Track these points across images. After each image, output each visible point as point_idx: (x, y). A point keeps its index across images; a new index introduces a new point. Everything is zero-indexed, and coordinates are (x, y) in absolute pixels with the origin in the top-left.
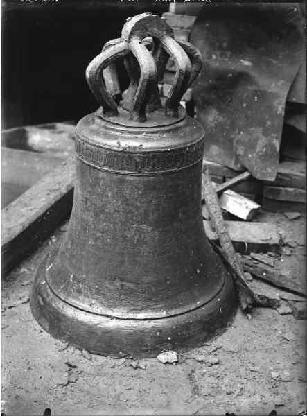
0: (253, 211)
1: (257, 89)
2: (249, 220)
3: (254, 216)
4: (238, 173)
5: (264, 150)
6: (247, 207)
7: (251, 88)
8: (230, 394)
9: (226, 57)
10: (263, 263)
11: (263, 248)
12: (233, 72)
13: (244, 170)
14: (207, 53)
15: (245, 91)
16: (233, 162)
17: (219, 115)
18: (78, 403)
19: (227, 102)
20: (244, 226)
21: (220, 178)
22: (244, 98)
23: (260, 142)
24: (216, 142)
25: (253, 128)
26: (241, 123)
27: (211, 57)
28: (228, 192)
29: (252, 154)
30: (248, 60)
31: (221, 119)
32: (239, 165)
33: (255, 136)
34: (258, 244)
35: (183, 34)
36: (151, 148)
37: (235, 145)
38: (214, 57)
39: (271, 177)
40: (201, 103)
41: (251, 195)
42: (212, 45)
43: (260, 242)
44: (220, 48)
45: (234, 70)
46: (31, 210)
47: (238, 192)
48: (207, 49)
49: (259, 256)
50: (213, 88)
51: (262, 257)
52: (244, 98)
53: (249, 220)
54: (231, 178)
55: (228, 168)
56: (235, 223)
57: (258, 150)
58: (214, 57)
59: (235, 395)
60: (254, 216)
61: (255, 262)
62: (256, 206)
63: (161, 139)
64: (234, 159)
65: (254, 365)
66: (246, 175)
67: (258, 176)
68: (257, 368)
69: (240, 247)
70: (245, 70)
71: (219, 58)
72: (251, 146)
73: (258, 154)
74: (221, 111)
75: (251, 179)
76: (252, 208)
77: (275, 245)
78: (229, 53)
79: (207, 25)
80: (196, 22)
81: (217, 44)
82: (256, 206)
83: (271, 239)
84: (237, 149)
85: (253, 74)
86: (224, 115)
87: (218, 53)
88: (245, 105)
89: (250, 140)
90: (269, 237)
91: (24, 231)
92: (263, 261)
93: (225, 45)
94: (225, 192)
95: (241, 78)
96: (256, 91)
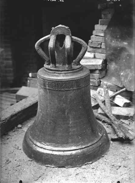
0: (126, 103)
1: (128, 54)
2: (124, 106)
3: (127, 105)
4: (122, 88)
5: (130, 79)
6: (123, 102)
7: (126, 53)
8: (93, 169)
9: (118, 41)
10: (125, 123)
11: (126, 118)
12: (119, 47)
13: (124, 87)
14: (111, 39)
15: (124, 54)
16: (120, 84)
17: (116, 65)
18: (35, 167)
19: (118, 60)
20: (120, 109)
21: (115, 90)
22: (124, 58)
23: (129, 75)
24: (114, 76)
25: (127, 70)
26: (123, 68)
27: (112, 42)
28: (118, 96)
29: (126, 80)
30: (127, 42)
31: (116, 67)
32: (122, 85)
33: (128, 73)
34: (124, 116)
35: (102, 33)
36: (64, 79)
37: (121, 77)
38: (113, 41)
39: (133, 89)
40: (109, 60)
41: (128, 98)
42: (113, 37)
43: (125, 115)
44: (116, 38)
45: (120, 46)
46: (35, 99)
47: (123, 96)
48: (110, 38)
49: (123, 121)
50: (113, 54)
51: (125, 121)
52: (124, 58)
53: (124, 106)
54: (119, 90)
55: (118, 86)
56: (117, 108)
57: (128, 78)
58: (113, 41)
59: (95, 169)
60: (127, 105)
61: (122, 123)
62: (128, 101)
63: (72, 75)
64: (120, 83)
65: (107, 160)
66: (124, 89)
67: (128, 90)
68: (107, 161)
69: (118, 117)
70: (125, 46)
71: (115, 42)
72: (126, 77)
73: (128, 80)
74: (116, 63)
75: (126, 91)
76: (125, 102)
77: (131, 116)
78: (120, 40)
79: (111, 29)
80: (107, 28)
81: (115, 36)
82: (128, 101)
83: (130, 114)
84: (121, 79)
85: (127, 47)
86: (118, 65)
87: (115, 40)
88: (124, 60)
89: (126, 74)
90: (129, 113)
91: (30, 106)
92: (125, 123)
93: (118, 36)
94: (116, 96)
95: (123, 49)
96: (128, 55)
